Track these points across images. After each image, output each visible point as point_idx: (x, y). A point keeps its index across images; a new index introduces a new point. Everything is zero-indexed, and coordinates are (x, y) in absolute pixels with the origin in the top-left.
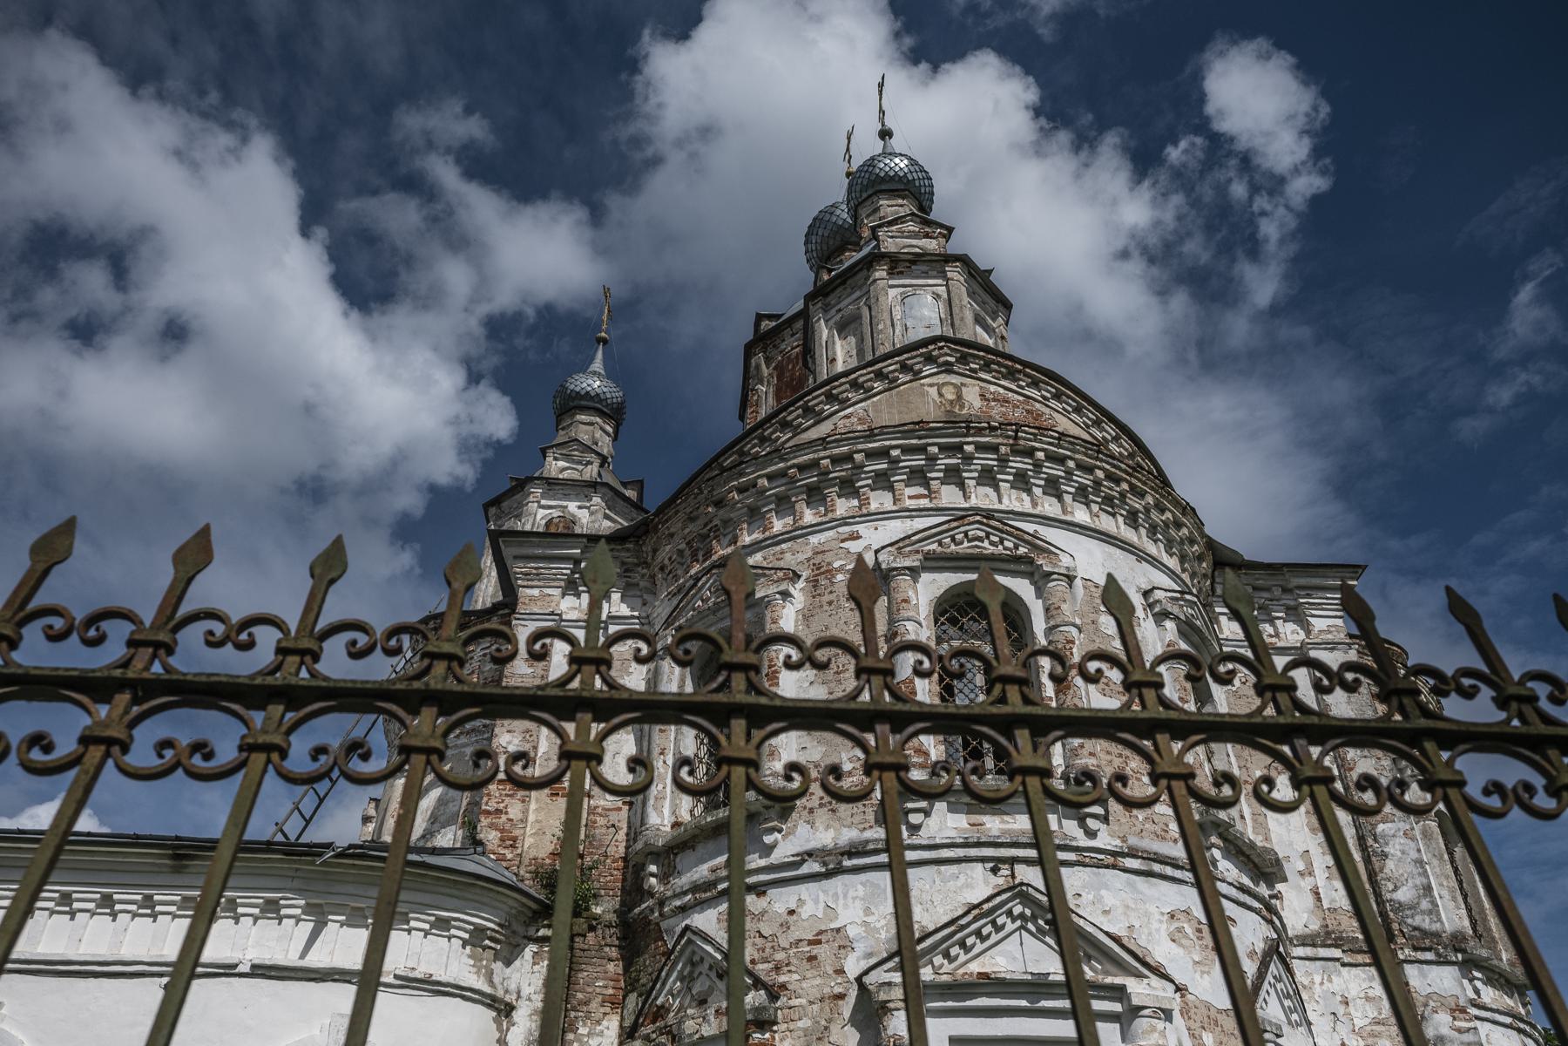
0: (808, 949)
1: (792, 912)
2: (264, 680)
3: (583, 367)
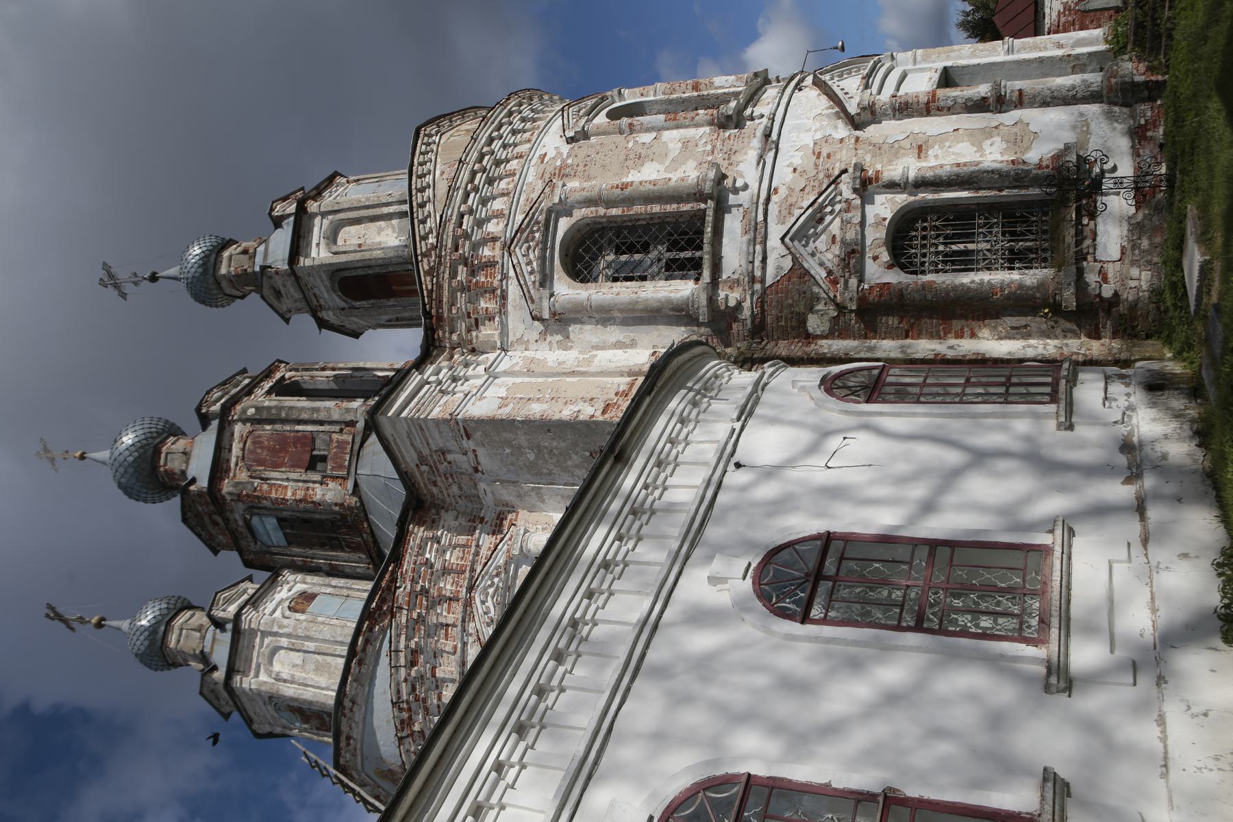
0: (822, 159)
1: (795, 170)
2: (693, 254)
3: (1165, 354)
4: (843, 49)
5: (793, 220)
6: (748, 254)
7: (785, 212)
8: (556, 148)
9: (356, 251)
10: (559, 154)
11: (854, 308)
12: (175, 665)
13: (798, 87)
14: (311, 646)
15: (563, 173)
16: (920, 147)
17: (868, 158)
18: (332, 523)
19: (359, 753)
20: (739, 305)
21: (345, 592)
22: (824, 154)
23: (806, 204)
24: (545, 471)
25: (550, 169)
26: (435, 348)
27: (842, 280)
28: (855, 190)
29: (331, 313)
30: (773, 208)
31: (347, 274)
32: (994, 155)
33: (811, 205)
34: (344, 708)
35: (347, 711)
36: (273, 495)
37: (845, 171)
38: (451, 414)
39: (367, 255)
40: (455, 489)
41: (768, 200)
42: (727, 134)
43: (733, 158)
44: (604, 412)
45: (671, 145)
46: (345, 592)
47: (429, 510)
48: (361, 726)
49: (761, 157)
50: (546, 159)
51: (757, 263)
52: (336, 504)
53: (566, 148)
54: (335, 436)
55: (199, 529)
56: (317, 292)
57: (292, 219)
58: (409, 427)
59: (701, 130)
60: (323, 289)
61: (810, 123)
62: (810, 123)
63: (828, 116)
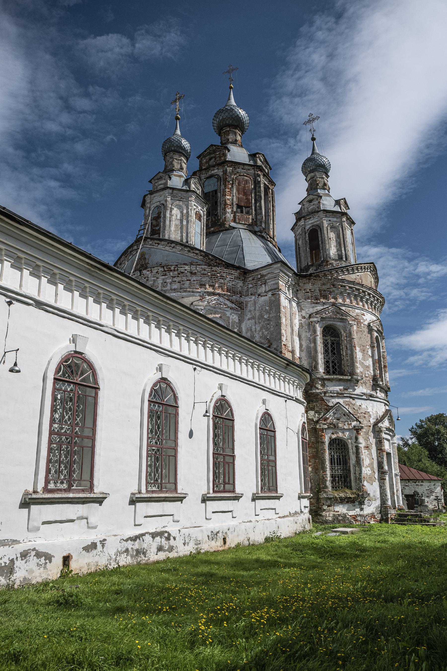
1: (360, 406)
4: (398, 420)
5: (345, 406)
6: (334, 391)
7: (347, 403)
8: (366, 319)
9: (328, 237)
10: (365, 321)
11: (317, 427)
12: (165, 155)
13: (386, 404)
14: (185, 223)
15: (359, 323)
16: (368, 447)
17: (364, 430)
18: (216, 215)
19: (152, 247)
20: (318, 388)
21: (202, 234)
22: (366, 415)
23: (350, 410)
24: (260, 321)
25: (360, 318)
26: (299, 278)
27: (325, 423)
28: (355, 426)
29: (303, 223)
30: (347, 399)
31: (319, 233)
32: (366, 471)
33: (350, 412)
34: (171, 244)
35: (170, 245)
36: (227, 190)
37: (360, 423)
38: (281, 289)
39: (327, 242)
40: (250, 286)
41: (351, 397)
42: (371, 381)
43: (364, 384)
44: (284, 345)
45: (367, 362)
46: (202, 234)
47: (244, 277)
48: (163, 249)
49: (364, 394)
50: (363, 316)
51: (331, 394)
52: (225, 218)
53: (366, 323)
54: (251, 217)
55: (208, 151)
56: (311, 219)
57: (340, 211)
58: (276, 273)
59: (372, 372)
60: (313, 221)
61: (375, 410)
62: (375, 410)
63: (377, 416)
